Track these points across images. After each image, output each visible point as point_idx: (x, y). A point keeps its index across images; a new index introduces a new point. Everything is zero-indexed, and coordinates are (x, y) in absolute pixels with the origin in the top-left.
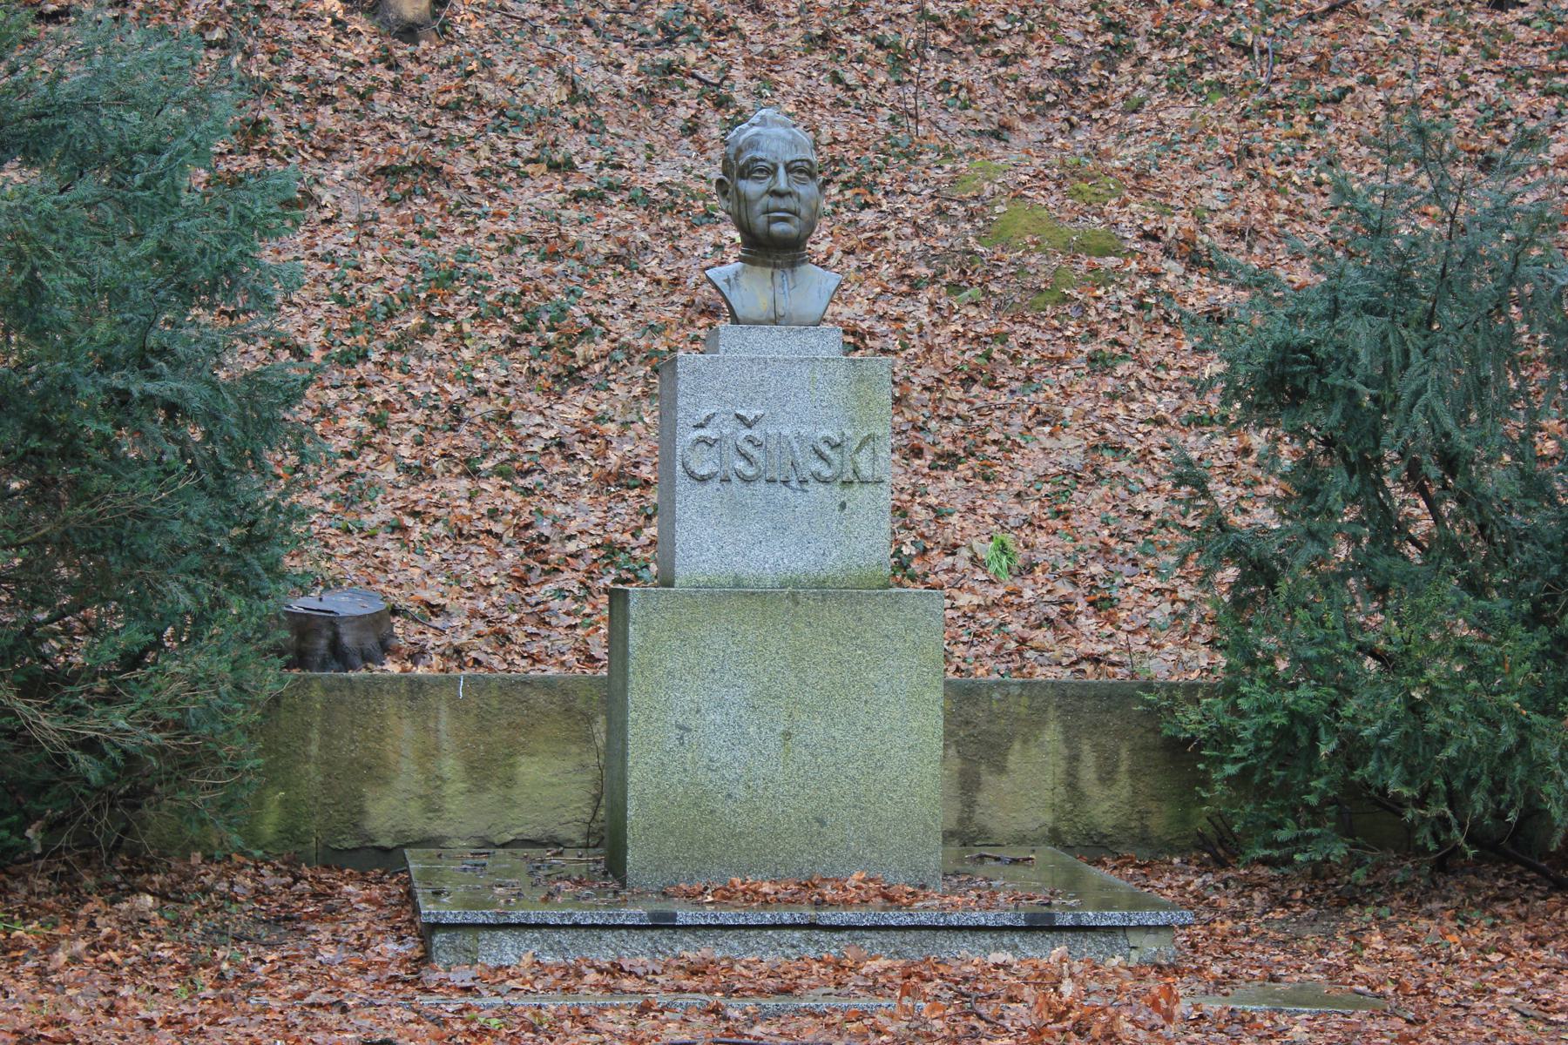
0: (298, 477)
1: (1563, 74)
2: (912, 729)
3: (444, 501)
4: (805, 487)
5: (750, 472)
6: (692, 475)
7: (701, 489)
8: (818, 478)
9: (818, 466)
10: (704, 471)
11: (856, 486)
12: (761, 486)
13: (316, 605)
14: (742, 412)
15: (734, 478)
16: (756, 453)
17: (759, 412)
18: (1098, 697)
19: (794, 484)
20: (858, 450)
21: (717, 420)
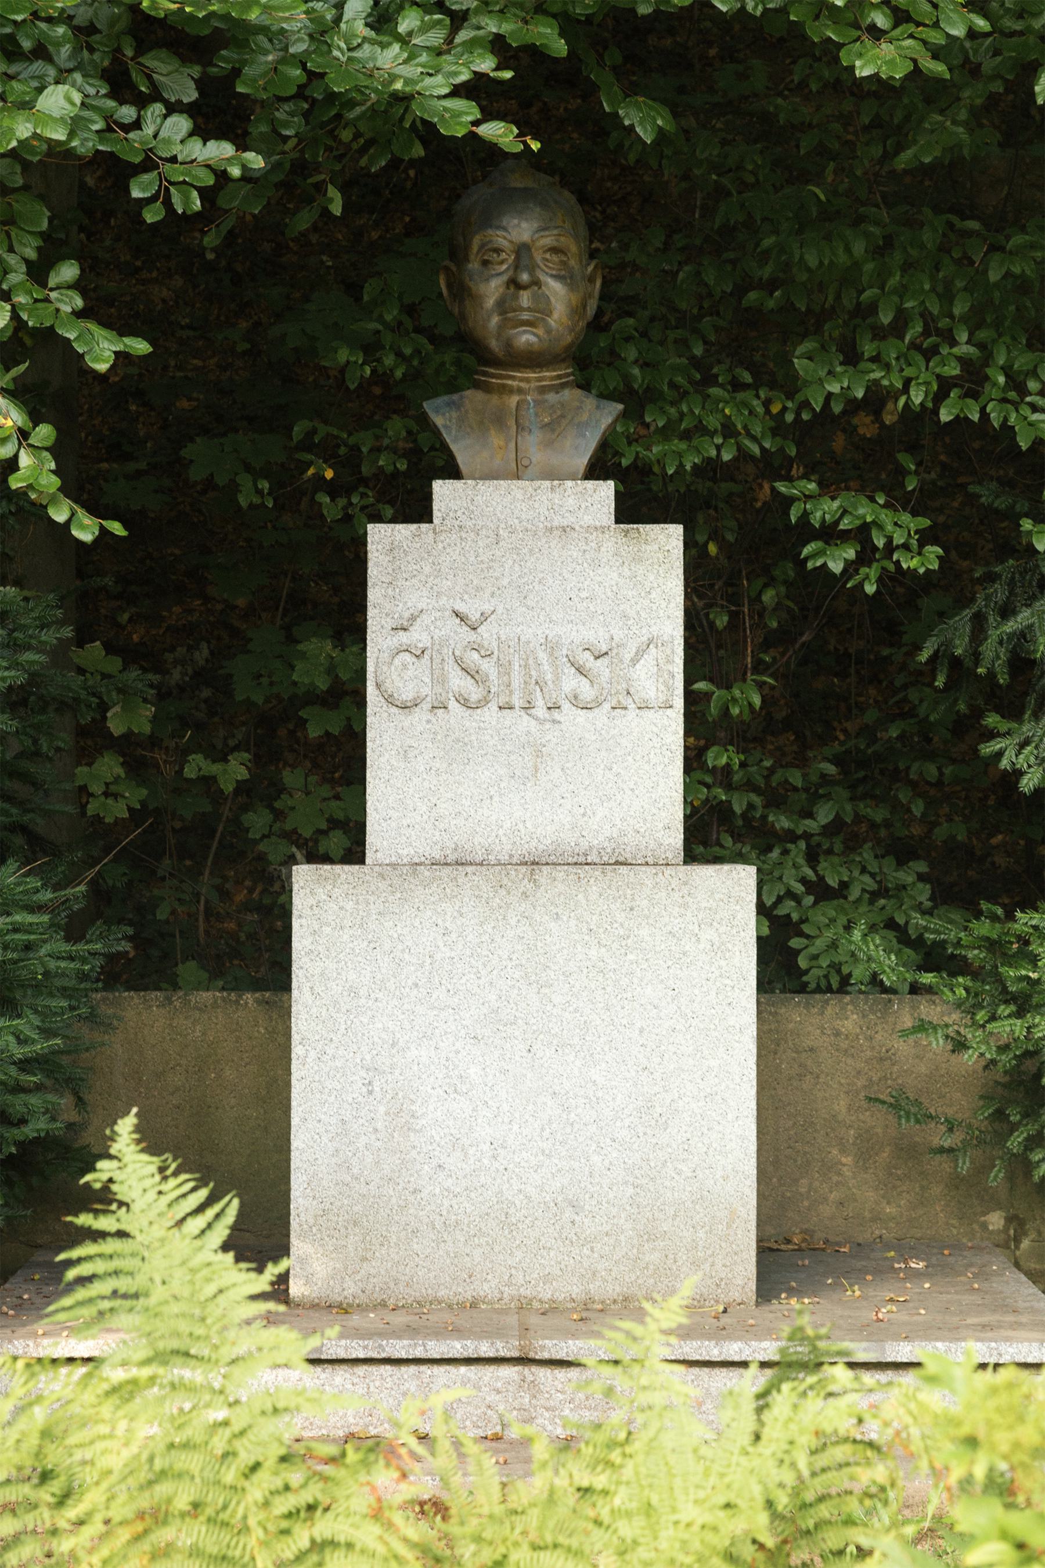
0: (994, 918)
1: (1042, 248)
2: (709, 1069)
3: (776, 874)
4: (556, 714)
5: (475, 694)
6: (390, 700)
7: (406, 720)
8: (575, 700)
9: (571, 682)
10: (407, 694)
11: (632, 713)
12: (490, 714)
13: (1003, 1347)
14: (461, 607)
15: (453, 704)
16: (488, 667)
17: (487, 608)
18: (845, 984)
19: (540, 711)
20: (635, 661)
21: (426, 619)
